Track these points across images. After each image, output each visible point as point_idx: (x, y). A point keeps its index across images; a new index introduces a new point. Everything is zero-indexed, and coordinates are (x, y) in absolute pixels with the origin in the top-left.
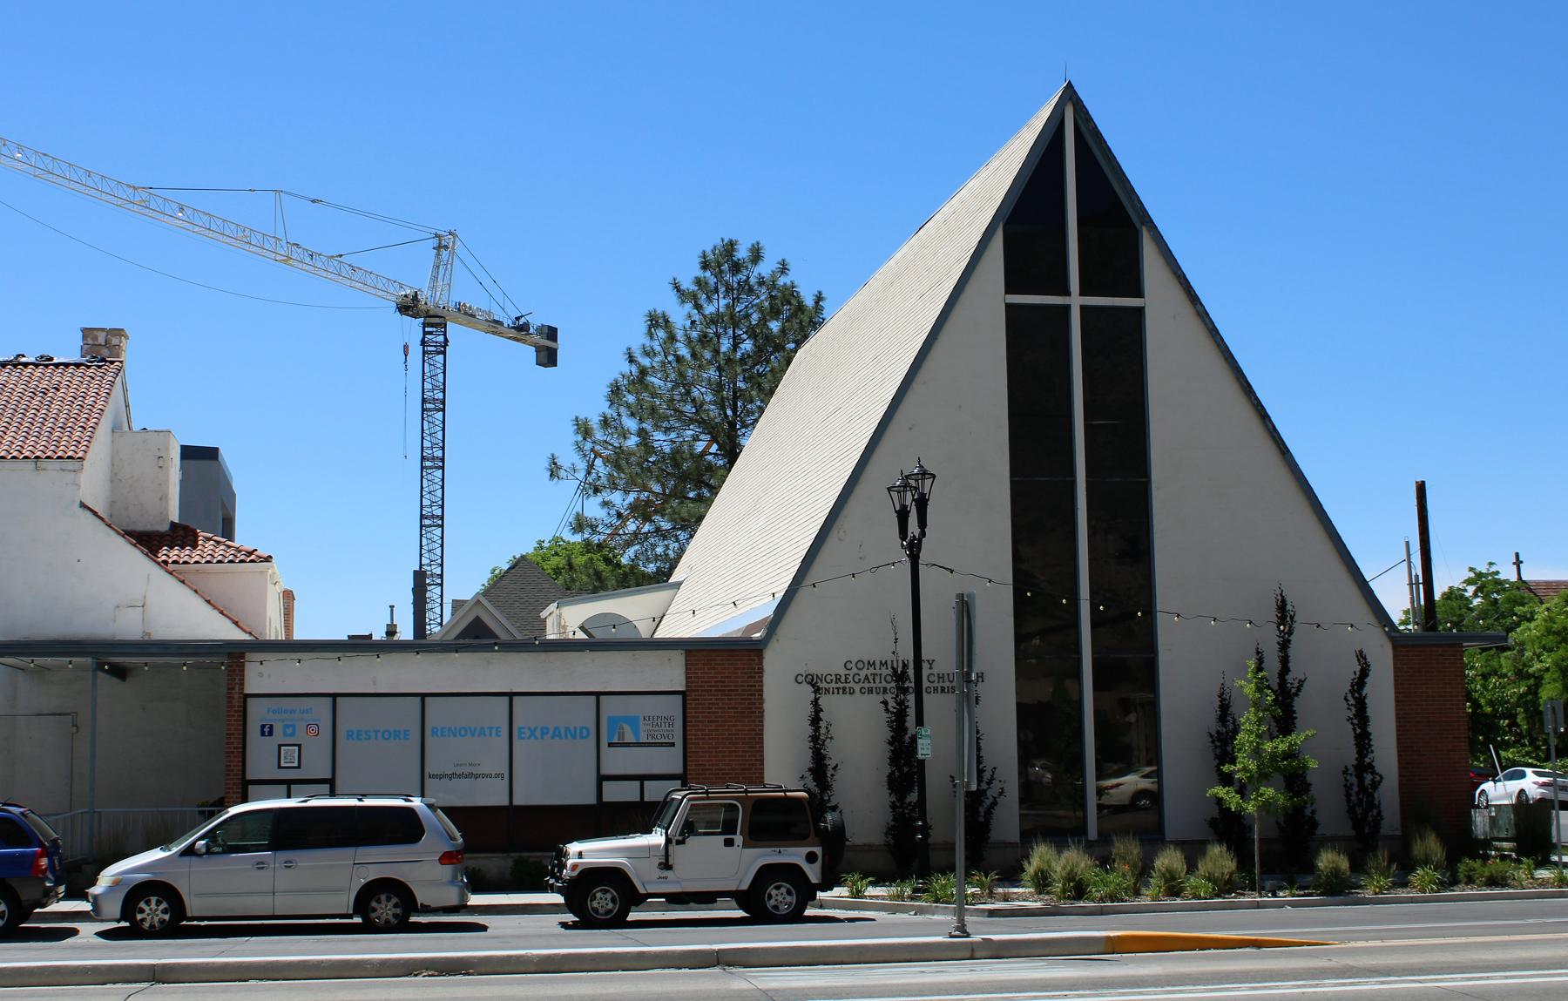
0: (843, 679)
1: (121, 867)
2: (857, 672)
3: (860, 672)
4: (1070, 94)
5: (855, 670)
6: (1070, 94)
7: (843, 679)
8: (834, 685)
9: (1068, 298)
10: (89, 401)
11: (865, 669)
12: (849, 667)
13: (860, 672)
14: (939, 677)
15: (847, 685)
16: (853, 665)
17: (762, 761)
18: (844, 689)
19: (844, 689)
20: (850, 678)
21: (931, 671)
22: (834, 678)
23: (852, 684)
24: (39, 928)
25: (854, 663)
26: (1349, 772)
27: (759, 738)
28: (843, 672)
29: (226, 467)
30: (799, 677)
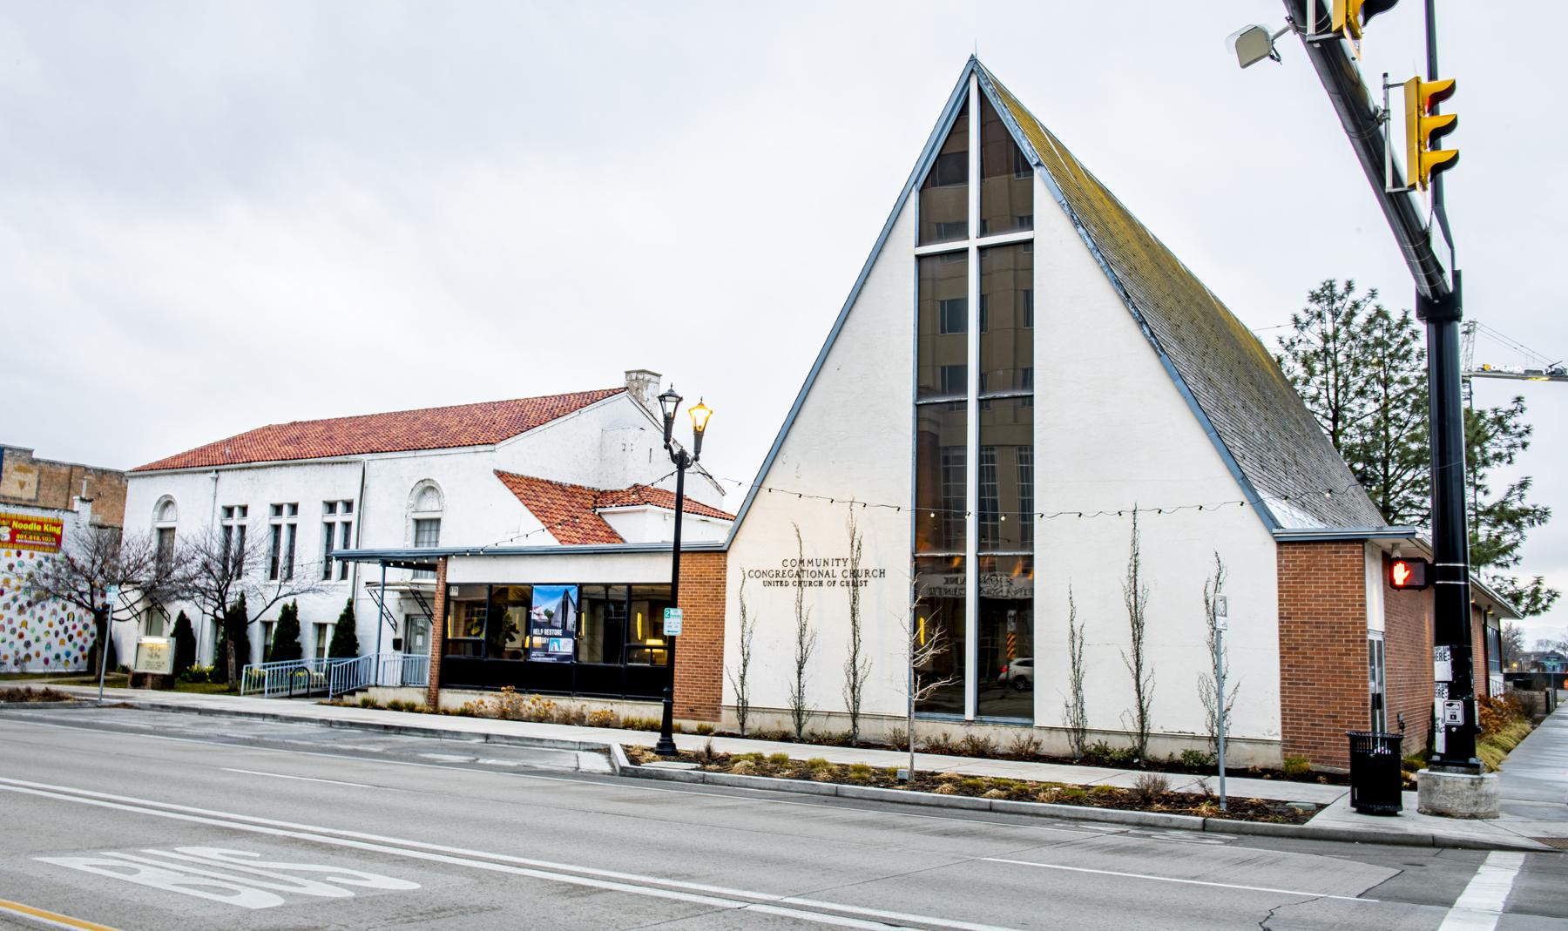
0: (781, 575)
1: (185, 699)
2: (791, 568)
3: (791, 568)
4: (974, 66)
5: (790, 568)
6: (974, 66)
7: (781, 575)
8: (774, 579)
9: (966, 242)
10: (529, 414)
11: (797, 566)
12: (785, 564)
13: (793, 569)
14: (881, 573)
15: (784, 580)
16: (788, 563)
17: (723, 637)
18: (782, 582)
19: (782, 582)
20: (786, 573)
21: (844, 568)
22: (774, 573)
23: (787, 579)
24: (1444, 580)
25: (789, 561)
26: (1325, 380)
27: (1283, 605)
28: (781, 568)
29: (912, 530)
30: (751, 573)
